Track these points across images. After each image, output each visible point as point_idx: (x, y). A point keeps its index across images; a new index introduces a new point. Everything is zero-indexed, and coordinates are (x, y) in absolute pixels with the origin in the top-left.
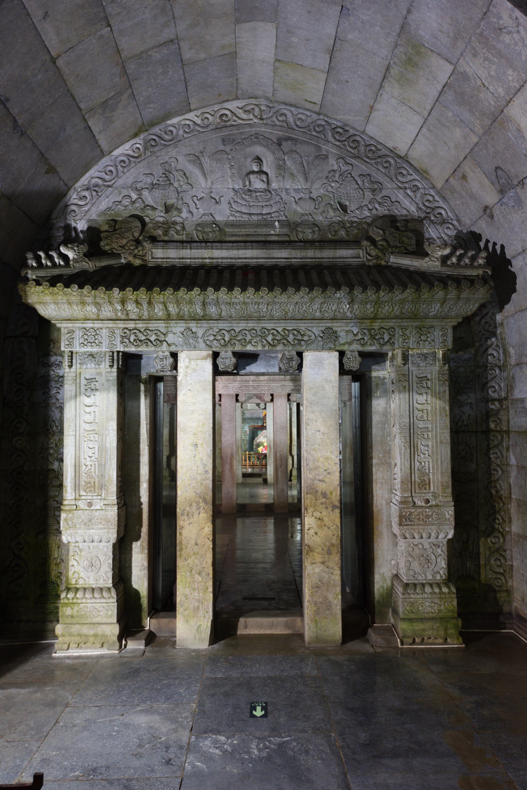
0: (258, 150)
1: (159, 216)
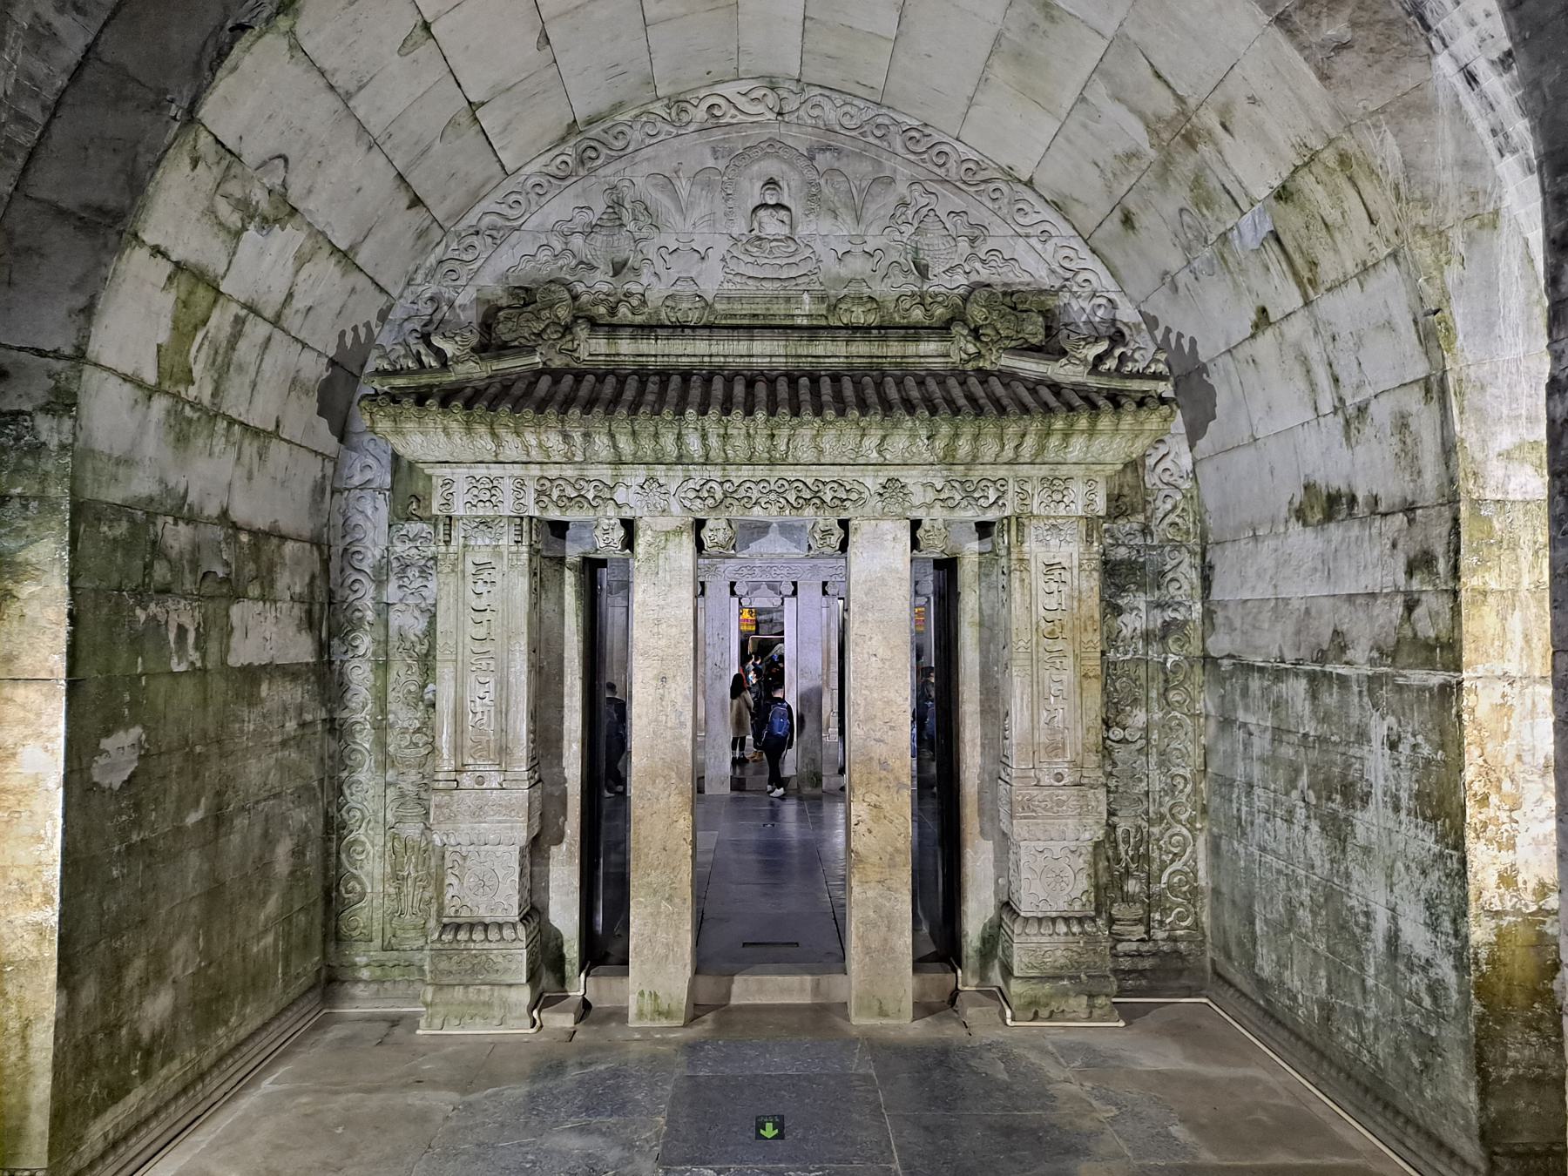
0: (772, 167)
1: (601, 282)
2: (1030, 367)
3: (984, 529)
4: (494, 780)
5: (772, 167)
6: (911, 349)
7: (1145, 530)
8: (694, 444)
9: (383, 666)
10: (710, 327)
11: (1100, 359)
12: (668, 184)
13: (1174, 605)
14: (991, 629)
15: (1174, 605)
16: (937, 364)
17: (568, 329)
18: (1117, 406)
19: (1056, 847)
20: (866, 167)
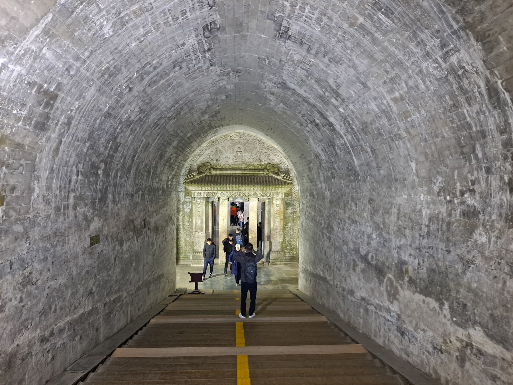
0: (239, 146)
1: (214, 162)
2: (275, 176)
3: (269, 199)
4: (201, 233)
5: (239, 146)
6: (259, 172)
7: (291, 198)
8: (228, 189)
9: (184, 217)
10: (230, 169)
11: (284, 176)
12: (224, 148)
13: (295, 209)
14: (269, 212)
15: (295, 209)
16: (262, 175)
17: (210, 169)
18: (285, 184)
19: (276, 242)
20: (253, 146)
